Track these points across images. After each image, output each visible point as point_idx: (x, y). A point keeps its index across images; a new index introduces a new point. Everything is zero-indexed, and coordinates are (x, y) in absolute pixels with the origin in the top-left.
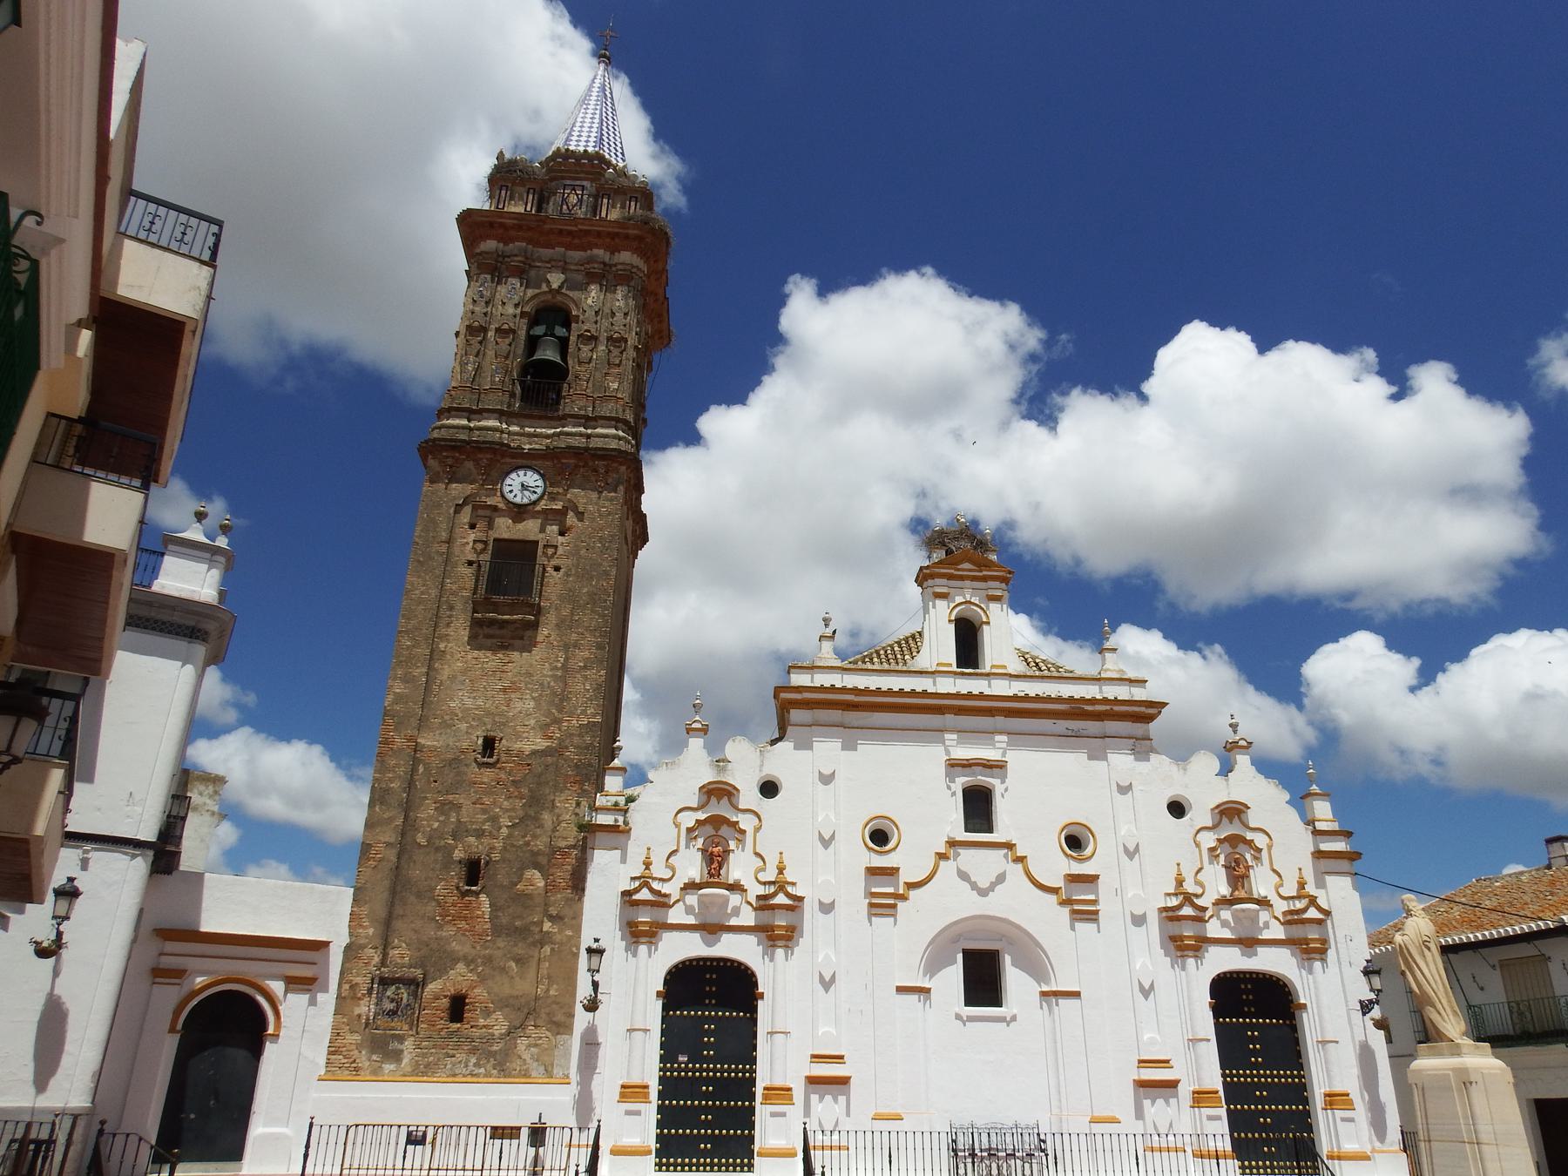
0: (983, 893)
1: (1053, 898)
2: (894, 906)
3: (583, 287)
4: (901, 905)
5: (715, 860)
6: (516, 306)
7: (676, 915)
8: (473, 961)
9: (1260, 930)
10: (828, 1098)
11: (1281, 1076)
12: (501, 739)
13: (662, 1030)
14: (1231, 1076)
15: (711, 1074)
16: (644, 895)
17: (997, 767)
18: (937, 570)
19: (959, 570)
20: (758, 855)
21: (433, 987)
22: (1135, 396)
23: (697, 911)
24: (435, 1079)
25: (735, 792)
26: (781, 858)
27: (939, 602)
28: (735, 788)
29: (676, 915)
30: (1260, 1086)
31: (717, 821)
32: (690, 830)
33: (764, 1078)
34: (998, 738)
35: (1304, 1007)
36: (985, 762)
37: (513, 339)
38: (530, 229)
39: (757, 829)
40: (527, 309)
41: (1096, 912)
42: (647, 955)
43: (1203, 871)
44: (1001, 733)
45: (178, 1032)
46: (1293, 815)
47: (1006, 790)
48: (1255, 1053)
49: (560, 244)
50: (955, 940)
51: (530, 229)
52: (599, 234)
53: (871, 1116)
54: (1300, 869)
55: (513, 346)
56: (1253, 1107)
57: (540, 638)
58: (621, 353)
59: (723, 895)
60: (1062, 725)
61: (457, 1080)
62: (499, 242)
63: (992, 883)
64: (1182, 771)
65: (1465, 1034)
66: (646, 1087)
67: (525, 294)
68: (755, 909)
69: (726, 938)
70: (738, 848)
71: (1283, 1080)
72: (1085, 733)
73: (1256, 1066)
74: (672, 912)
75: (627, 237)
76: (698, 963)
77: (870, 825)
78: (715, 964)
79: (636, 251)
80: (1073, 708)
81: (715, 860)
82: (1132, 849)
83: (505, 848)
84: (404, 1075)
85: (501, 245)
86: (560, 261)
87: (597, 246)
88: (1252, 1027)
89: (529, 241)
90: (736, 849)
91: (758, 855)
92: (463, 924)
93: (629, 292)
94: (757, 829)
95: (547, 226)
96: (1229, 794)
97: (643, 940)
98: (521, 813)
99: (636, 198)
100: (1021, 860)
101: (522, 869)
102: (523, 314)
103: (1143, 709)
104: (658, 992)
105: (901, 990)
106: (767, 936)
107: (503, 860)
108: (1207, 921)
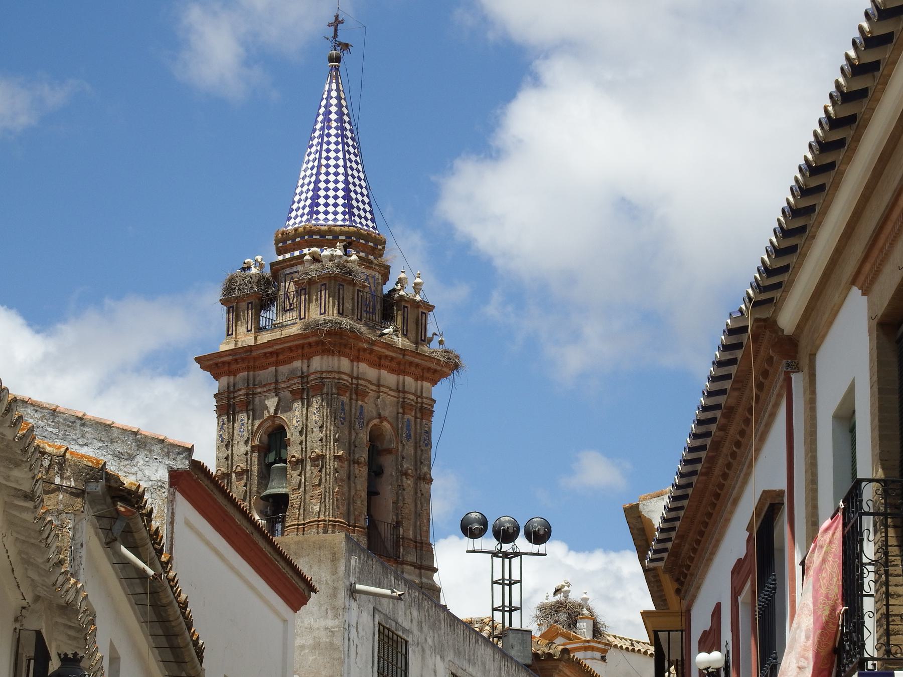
3: (288, 409)
6: (246, 442)
22: (490, 646)
37: (247, 480)
38: (243, 359)
40: (256, 442)
49: (270, 365)
52: (290, 349)
55: (248, 486)
58: (320, 471)
62: (229, 376)
65: (833, 171)
67: (253, 425)
75: (310, 344)
85: (232, 378)
86: (271, 384)
89: (248, 369)
93: (322, 401)
95: (254, 354)
99: (325, 284)
102: (253, 448)
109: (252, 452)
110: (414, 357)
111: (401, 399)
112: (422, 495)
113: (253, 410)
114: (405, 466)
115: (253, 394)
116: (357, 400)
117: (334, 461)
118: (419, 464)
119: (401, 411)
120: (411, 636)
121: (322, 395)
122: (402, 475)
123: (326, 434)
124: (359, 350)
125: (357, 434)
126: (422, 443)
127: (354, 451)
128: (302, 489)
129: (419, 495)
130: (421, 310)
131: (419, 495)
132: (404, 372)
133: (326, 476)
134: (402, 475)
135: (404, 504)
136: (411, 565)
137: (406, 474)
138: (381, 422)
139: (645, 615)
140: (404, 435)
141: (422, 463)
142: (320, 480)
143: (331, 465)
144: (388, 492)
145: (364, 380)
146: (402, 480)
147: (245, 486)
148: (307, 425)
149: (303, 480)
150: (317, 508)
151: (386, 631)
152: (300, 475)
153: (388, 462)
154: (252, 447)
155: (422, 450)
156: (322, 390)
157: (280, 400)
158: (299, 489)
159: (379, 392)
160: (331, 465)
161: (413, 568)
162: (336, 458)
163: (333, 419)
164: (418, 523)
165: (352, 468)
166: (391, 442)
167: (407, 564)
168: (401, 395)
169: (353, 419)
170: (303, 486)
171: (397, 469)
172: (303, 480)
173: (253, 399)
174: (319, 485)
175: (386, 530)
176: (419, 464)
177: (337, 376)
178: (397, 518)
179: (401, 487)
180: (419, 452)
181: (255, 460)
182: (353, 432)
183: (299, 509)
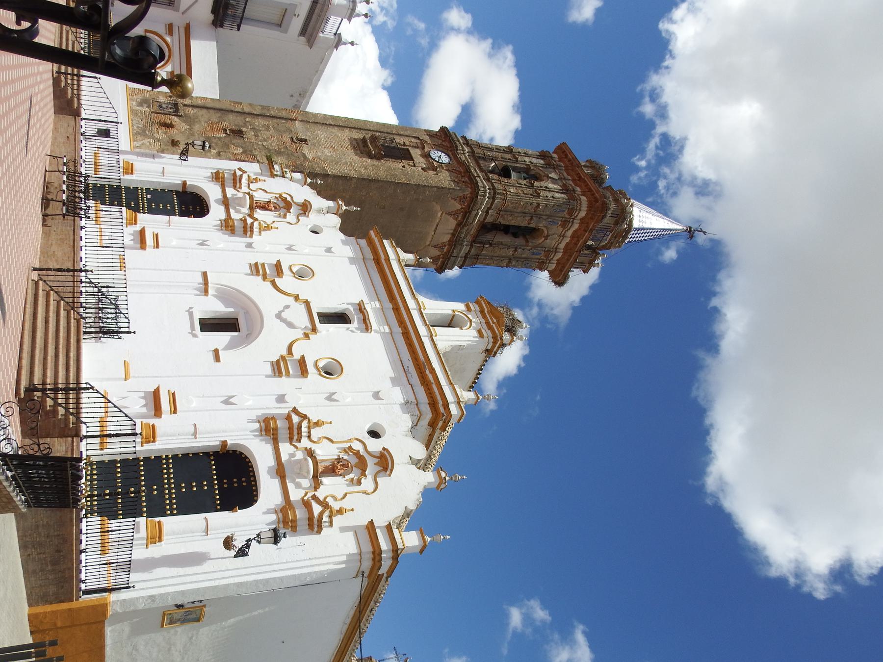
0: (279, 316)
1: (284, 352)
4: (260, 278)
7: (286, 449)
9: (293, 481)
11: (170, 495)
12: (307, 144)
13: (198, 453)
14: (171, 509)
16: (317, 509)
17: (366, 326)
20: (346, 495)
21: (176, 118)
23: (292, 459)
24: (130, 115)
27: (475, 334)
28: (392, 470)
29: (286, 449)
30: (161, 490)
31: (362, 464)
32: (350, 448)
33: (170, 523)
34: (377, 303)
35: (184, 183)
36: (367, 317)
38: (572, 164)
39: (365, 493)
41: (280, 374)
42: (206, 176)
43: (331, 443)
45: (145, 34)
47: (352, 331)
48: (189, 487)
50: (247, 313)
51: (572, 164)
54: (331, 423)
56: (143, 483)
57: (364, 159)
58: (531, 195)
59: (246, 203)
60: (410, 364)
61: (128, 95)
64: (404, 433)
66: (132, 173)
69: (276, 482)
71: (165, 471)
72: (409, 376)
73: (178, 487)
75: (593, 194)
76: (251, 471)
77: (308, 269)
79: (589, 201)
80: (423, 363)
84: (131, 107)
88: (211, 485)
90: (345, 479)
91: (346, 495)
92: (208, 129)
93: (566, 199)
94: (365, 493)
96: (398, 464)
97: (280, 515)
100: (306, 336)
101: (242, 147)
103: (441, 403)
105: (205, 275)
107: (245, 142)
109: (526, 165)
110: (574, 258)
111: (552, 250)
112: (502, 261)
114: (519, 250)
115: (554, 168)
116: (561, 221)
117: (537, 203)
118: (517, 259)
119: (546, 249)
121: (569, 199)
122: (515, 248)
123: (549, 200)
124: (587, 223)
125: (545, 220)
126: (527, 262)
127: (537, 217)
128: (518, 185)
129: (502, 259)
130: (587, 265)
131: (502, 259)
132: (565, 252)
133: (529, 197)
134: (515, 248)
135: (500, 249)
136: (469, 251)
137: (516, 250)
139: (391, 378)
140: (534, 251)
141: (517, 261)
142: (527, 194)
143: (535, 201)
144: (507, 239)
145: (571, 226)
146: (513, 248)
148: (550, 191)
149: (523, 186)
150: (512, 191)
152: (525, 185)
153: (520, 241)
155: (523, 262)
156: (571, 199)
157: (556, 180)
158: (518, 183)
159: (560, 236)
160: (535, 201)
161: (467, 252)
162: (538, 204)
163: (557, 204)
164: (487, 257)
165: (529, 215)
167: (470, 248)
168: (554, 250)
169: (553, 218)
170: (520, 186)
171: (518, 246)
172: (523, 186)
174: (524, 193)
175: (489, 237)
176: (517, 259)
177: (578, 208)
178: (494, 244)
179: (509, 247)
180: (523, 260)
181: (522, 166)
182: (546, 217)
183: (507, 183)
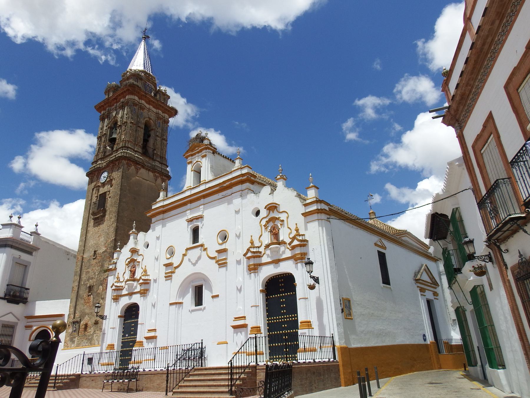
0: (194, 265)
1: (214, 261)
2: (171, 276)
4: (173, 275)
5: (275, 234)
8: (89, 314)
9: (281, 255)
10: (239, 334)
14: (295, 317)
15: (270, 321)
17: (201, 217)
18: (187, 155)
19: (196, 150)
20: (289, 228)
21: (82, 323)
25: (277, 206)
26: (251, 238)
28: (276, 204)
29: (265, 259)
30: (284, 323)
32: (265, 226)
38: (107, 103)
39: (288, 218)
44: (201, 205)
46: (298, 200)
47: (203, 225)
49: (115, 103)
53: (217, 343)
58: (125, 127)
60: (220, 195)
63: (196, 260)
68: (290, 250)
69: (282, 264)
70: (281, 228)
72: (227, 195)
73: (284, 314)
74: (263, 258)
75: (125, 92)
76: (283, 275)
78: (277, 277)
81: (275, 234)
82: (238, 235)
83: (96, 281)
87: (121, 99)
88: (282, 297)
91: (289, 228)
94: (288, 218)
98: (99, 270)
101: (99, 286)
103: (241, 178)
104: (118, 316)
106: (294, 260)
107: (96, 284)
108: (262, 257)
109: (108, 129)
113: (109, 118)
114: (158, 134)
120: (290, 248)
121: (128, 106)
129: (163, 144)
131: (163, 144)
136: (158, 162)
138: (150, 120)
142: (125, 129)
144: (151, 141)
145: (143, 105)
147: (105, 138)
150: (123, 137)
151: (524, 277)
152: (120, 130)
153: (152, 133)
154: (108, 127)
159: (149, 111)
160: (129, 125)
162: (131, 123)
166: (153, 127)
173: (110, 115)
174: (125, 131)
177: (133, 100)
179: (156, 140)
180: (163, 132)
181: (109, 131)
